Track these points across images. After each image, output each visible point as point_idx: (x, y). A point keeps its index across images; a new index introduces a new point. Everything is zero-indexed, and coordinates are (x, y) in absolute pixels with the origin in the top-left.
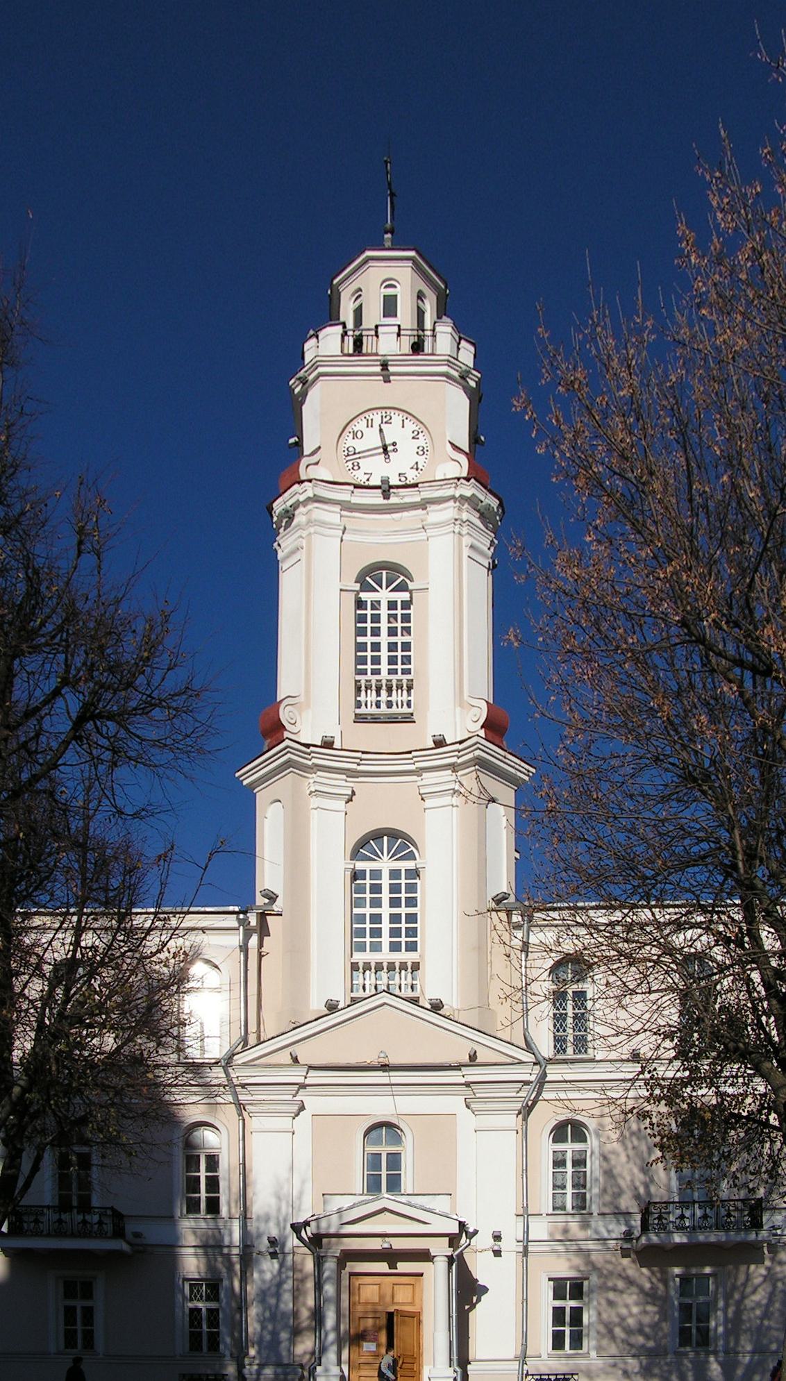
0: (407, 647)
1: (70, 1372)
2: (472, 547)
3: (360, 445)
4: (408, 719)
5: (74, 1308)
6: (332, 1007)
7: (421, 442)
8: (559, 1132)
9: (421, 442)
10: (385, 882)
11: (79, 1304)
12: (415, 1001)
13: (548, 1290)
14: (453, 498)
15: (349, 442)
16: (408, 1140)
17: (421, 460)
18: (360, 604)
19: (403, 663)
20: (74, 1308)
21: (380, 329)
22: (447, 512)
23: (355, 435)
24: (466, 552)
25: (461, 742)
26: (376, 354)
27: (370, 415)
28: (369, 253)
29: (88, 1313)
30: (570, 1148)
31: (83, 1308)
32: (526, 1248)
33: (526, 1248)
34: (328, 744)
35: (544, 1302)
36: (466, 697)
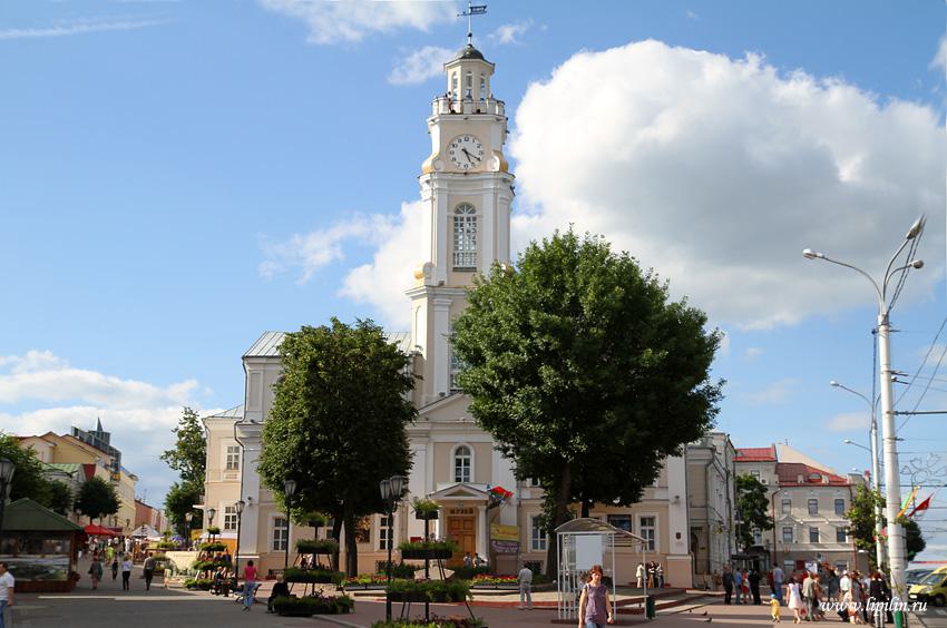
6: (442, 394)
13: (271, 523)
18: (456, 219)
34: (442, 284)
35: (270, 528)
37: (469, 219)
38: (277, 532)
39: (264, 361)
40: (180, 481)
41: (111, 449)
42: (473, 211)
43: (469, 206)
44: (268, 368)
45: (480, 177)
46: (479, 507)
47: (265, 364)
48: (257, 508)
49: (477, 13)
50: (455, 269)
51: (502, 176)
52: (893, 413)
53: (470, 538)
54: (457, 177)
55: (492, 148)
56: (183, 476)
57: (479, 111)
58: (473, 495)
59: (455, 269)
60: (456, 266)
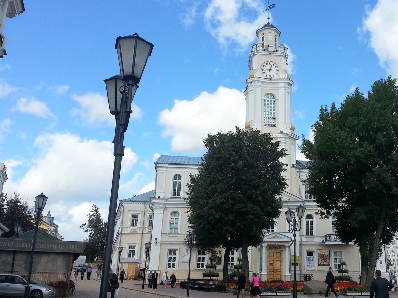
0: (274, 110)
1: (50, 286)
2: (288, 92)
3: (265, 68)
4: (274, 126)
5: (200, 257)
7: (277, 69)
8: (307, 217)
9: (277, 69)
10: (269, 103)
11: (172, 256)
12: (104, 264)
13: (305, 253)
14: (284, 82)
15: (263, 68)
16: (183, 179)
17: (277, 72)
19: (267, 104)
20: (200, 257)
21: (269, 46)
22: (283, 85)
23: (264, 66)
24: (287, 93)
25: (286, 133)
26: (269, 51)
27: (267, 63)
28: (266, 28)
29: (174, 258)
30: (309, 220)
31: (202, 257)
32: (301, 244)
33: (301, 244)
36: (287, 122)
37: (271, 101)
38: (170, 258)
39: (166, 165)
40: (88, 238)
41: (54, 224)
42: (274, 97)
43: (271, 95)
44: (168, 169)
45: (278, 81)
46: (286, 245)
47: (167, 167)
48: (159, 245)
49: (272, 8)
50: (265, 125)
51: (288, 81)
52: (12, 272)
53: (279, 262)
54: (266, 81)
55: (283, 69)
56: (90, 236)
57: (277, 51)
58: (281, 238)
59: (265, 125)
60: (266, 123)
